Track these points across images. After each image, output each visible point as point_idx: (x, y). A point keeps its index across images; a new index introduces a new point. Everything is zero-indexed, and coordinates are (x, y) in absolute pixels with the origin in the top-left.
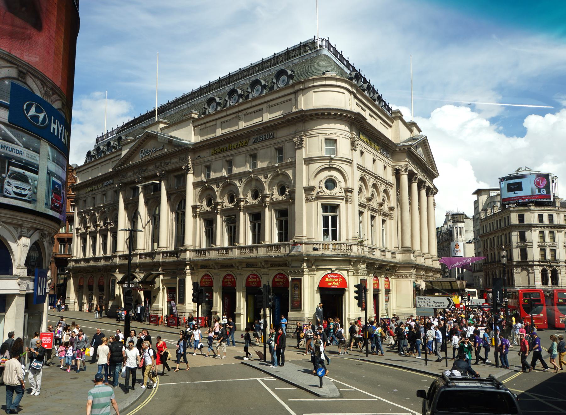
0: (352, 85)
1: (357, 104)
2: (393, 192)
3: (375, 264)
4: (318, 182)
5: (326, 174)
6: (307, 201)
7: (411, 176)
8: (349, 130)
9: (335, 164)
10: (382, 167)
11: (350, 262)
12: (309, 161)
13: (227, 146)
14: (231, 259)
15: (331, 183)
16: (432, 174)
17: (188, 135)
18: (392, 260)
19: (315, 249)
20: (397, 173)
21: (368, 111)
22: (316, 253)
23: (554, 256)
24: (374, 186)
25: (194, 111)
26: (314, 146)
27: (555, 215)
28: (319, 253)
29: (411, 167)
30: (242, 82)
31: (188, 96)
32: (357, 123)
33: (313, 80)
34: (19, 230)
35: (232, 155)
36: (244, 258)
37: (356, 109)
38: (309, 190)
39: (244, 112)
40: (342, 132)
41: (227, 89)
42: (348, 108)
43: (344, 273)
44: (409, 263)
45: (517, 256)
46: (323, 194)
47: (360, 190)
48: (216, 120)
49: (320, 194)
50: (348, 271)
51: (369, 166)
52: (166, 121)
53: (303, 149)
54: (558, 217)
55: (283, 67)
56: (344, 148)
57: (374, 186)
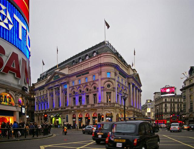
0: (115, 56)
2: (128, 90)
5: (107, 83)
7: (133, 85)
8: (114, 69)
10: (124, 82)
15: (109, 86)
17: (66, 71)
20: (129, 84)
21: (120, 64)
23: (174, 110)
24: (122, 87)
29: (134, 82)
30: (83, 55)
32: (116, 67)
35: (80, 78)
37: (116, 63)
39: (83, 65)
41: (78, 58)
42: (112, 62)
47: (118, 88)
48: (75, 67)
51: (120, 81)
54: (176, 100)
57: (122, 87)
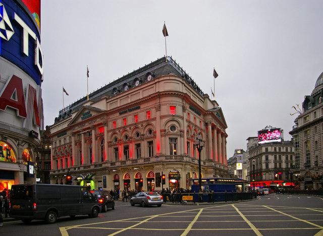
7: (213, 127)
10: (198, 121)
15: (173, 128)
16: (225, 126)
20: (206, 124)
21: (192, 93)
24: (195, 130)
27: (282, 148)
29: (214, 122)
30: (130, 80)
32: (185, 97)
34: (17, 142)
37: (185, 91)
42: (178, 90)
45: (264, 166)
47: (188, 131)
50: (182, 169)
54: (283, 149)
56: (179, 111)
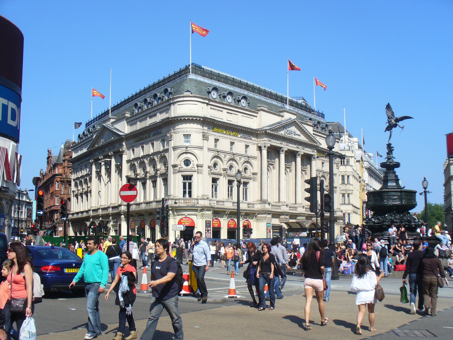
1: (211, 108)
3: (225, 211)
4: (180, 162)
5: (184, 156)
6: (174, 173)
9: (189, 150)
11: (197, 210)
12: (175, 148)
13: (142, 136)
14: (150, 209)
17: (124, 128)
18: (248, 209)
19: (176, 203)
22: (176, 205)
25: (127, 112)
26: (177, 138)
28: (177, 205)
31: (172, 76)
33: (177, 98)
36: (147, 210)
38: (174, 166)
40: (194, 130)
43: (194, 218)
44: (263, 211)
46: (182, 169)
48: (137, 119)
49: (180, 169)
52: (115, 117)
53: (172, 141)
55: (155, 93)
